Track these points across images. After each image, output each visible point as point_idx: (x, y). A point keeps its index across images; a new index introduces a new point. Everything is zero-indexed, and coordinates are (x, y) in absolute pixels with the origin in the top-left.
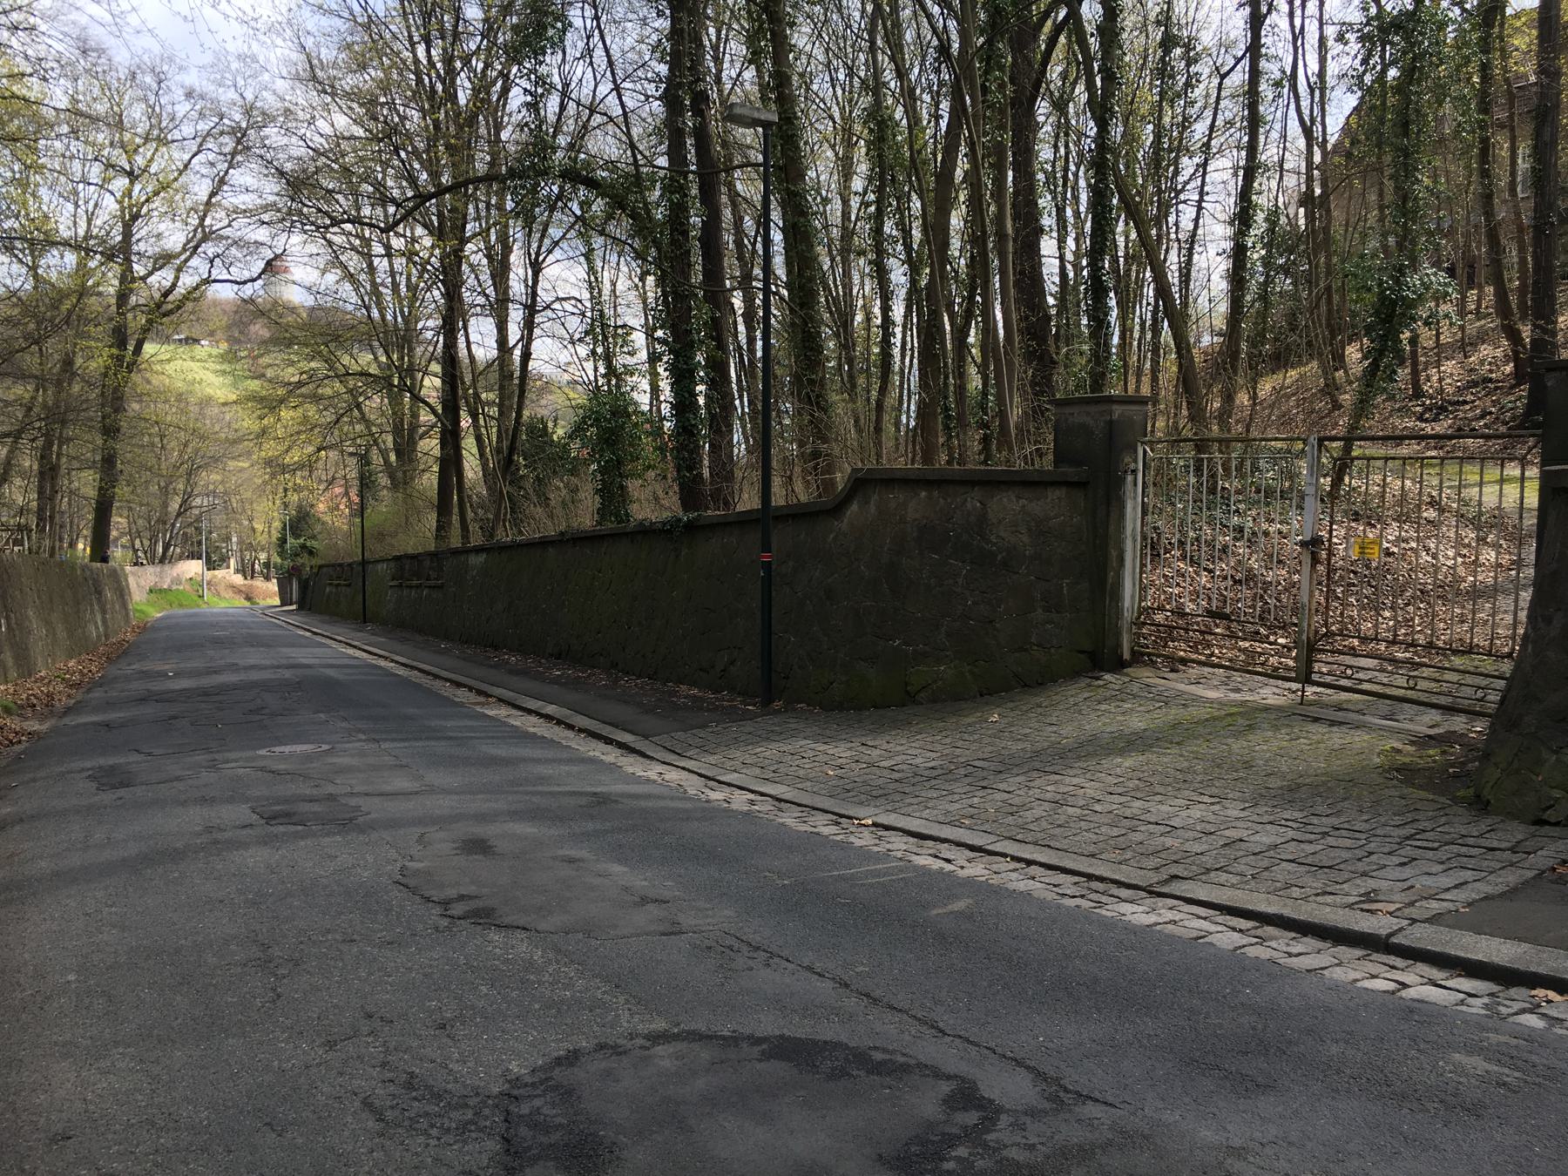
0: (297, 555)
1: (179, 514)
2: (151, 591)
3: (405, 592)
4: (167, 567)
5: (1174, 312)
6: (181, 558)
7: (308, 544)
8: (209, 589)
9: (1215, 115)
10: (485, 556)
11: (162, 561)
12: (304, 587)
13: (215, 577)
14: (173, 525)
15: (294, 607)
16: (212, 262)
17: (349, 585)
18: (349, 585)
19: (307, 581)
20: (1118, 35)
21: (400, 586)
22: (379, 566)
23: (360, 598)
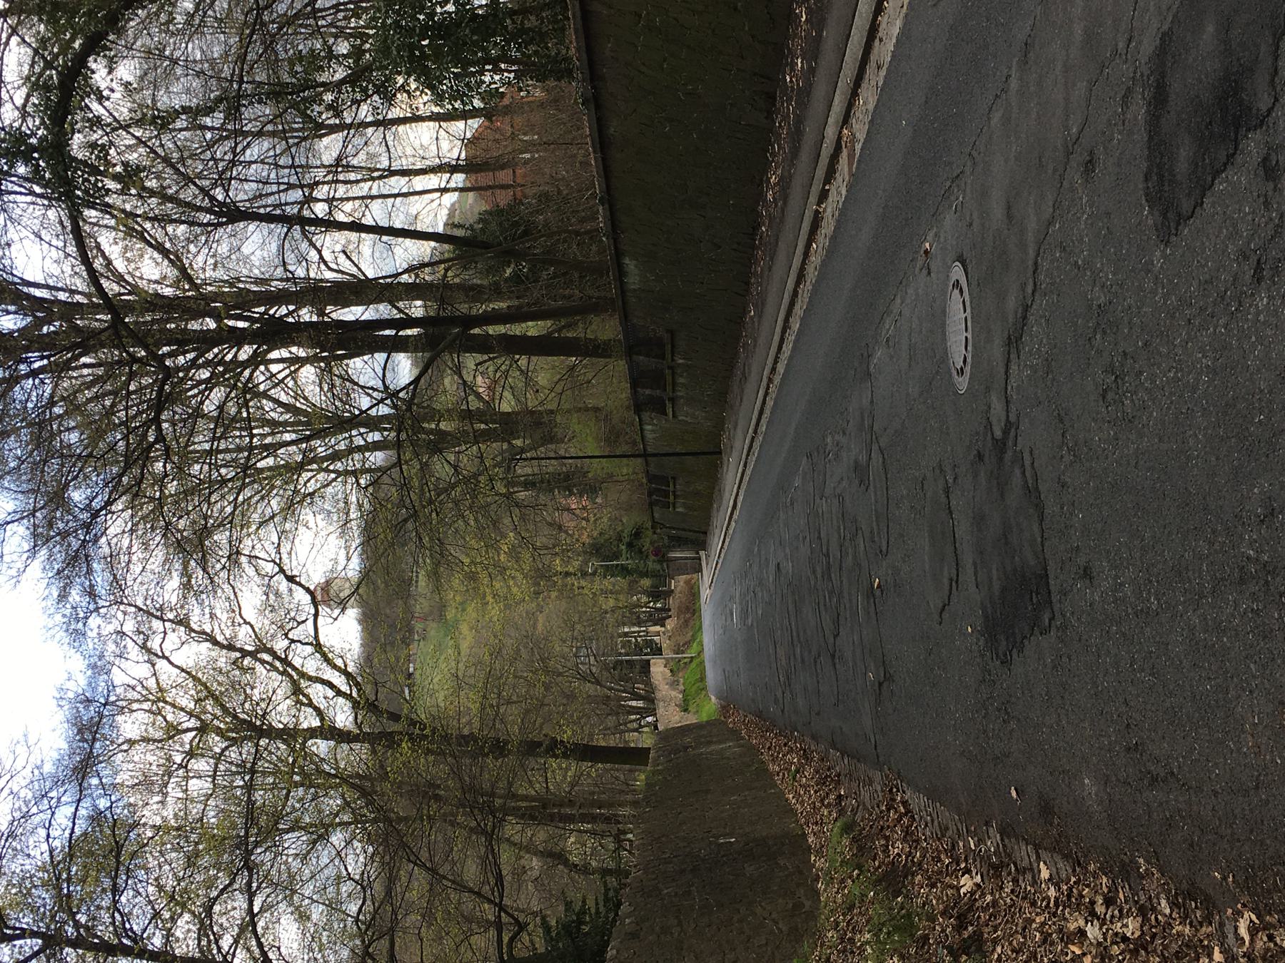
0: (641, 552)
1: (598, 682)
2: (686, 710)
3: (681, 393)
4: (658, 695)
5: (1045, 863)
6: (648, 683)
7: (627, 540)
8: (683, 652)
9: (549, 458)
10: (627, 261)
11: (652, 701)
12: (679, 542)
13: (669, 646)
14: (611, 689)
15: (702, 553)
16: (293, 641)
17: (674, 478)
18: (674, 478)
19: (671, 538)
20: (362, 544)
21: (672, 400)
22: (649, 436)
23: (690, 460)
